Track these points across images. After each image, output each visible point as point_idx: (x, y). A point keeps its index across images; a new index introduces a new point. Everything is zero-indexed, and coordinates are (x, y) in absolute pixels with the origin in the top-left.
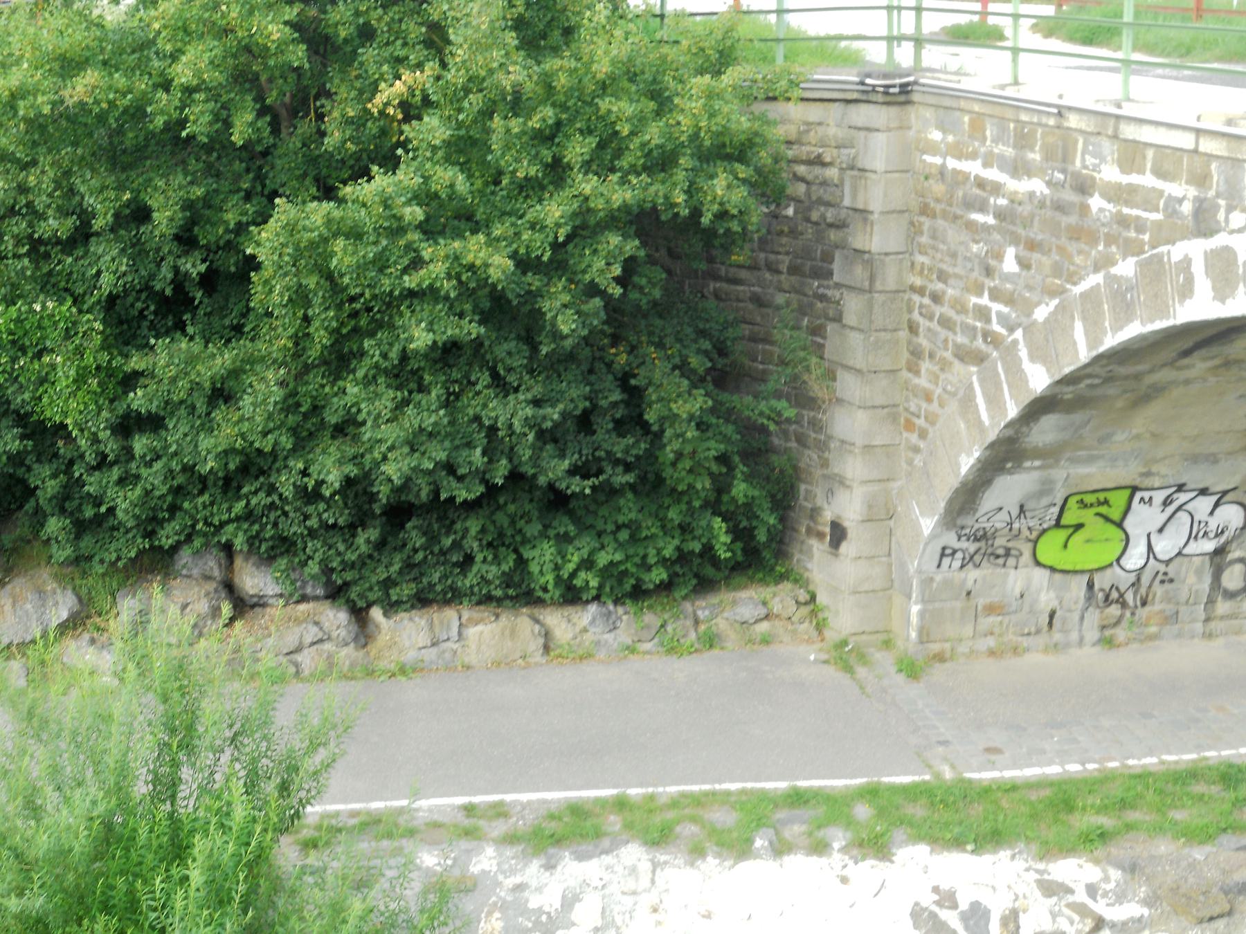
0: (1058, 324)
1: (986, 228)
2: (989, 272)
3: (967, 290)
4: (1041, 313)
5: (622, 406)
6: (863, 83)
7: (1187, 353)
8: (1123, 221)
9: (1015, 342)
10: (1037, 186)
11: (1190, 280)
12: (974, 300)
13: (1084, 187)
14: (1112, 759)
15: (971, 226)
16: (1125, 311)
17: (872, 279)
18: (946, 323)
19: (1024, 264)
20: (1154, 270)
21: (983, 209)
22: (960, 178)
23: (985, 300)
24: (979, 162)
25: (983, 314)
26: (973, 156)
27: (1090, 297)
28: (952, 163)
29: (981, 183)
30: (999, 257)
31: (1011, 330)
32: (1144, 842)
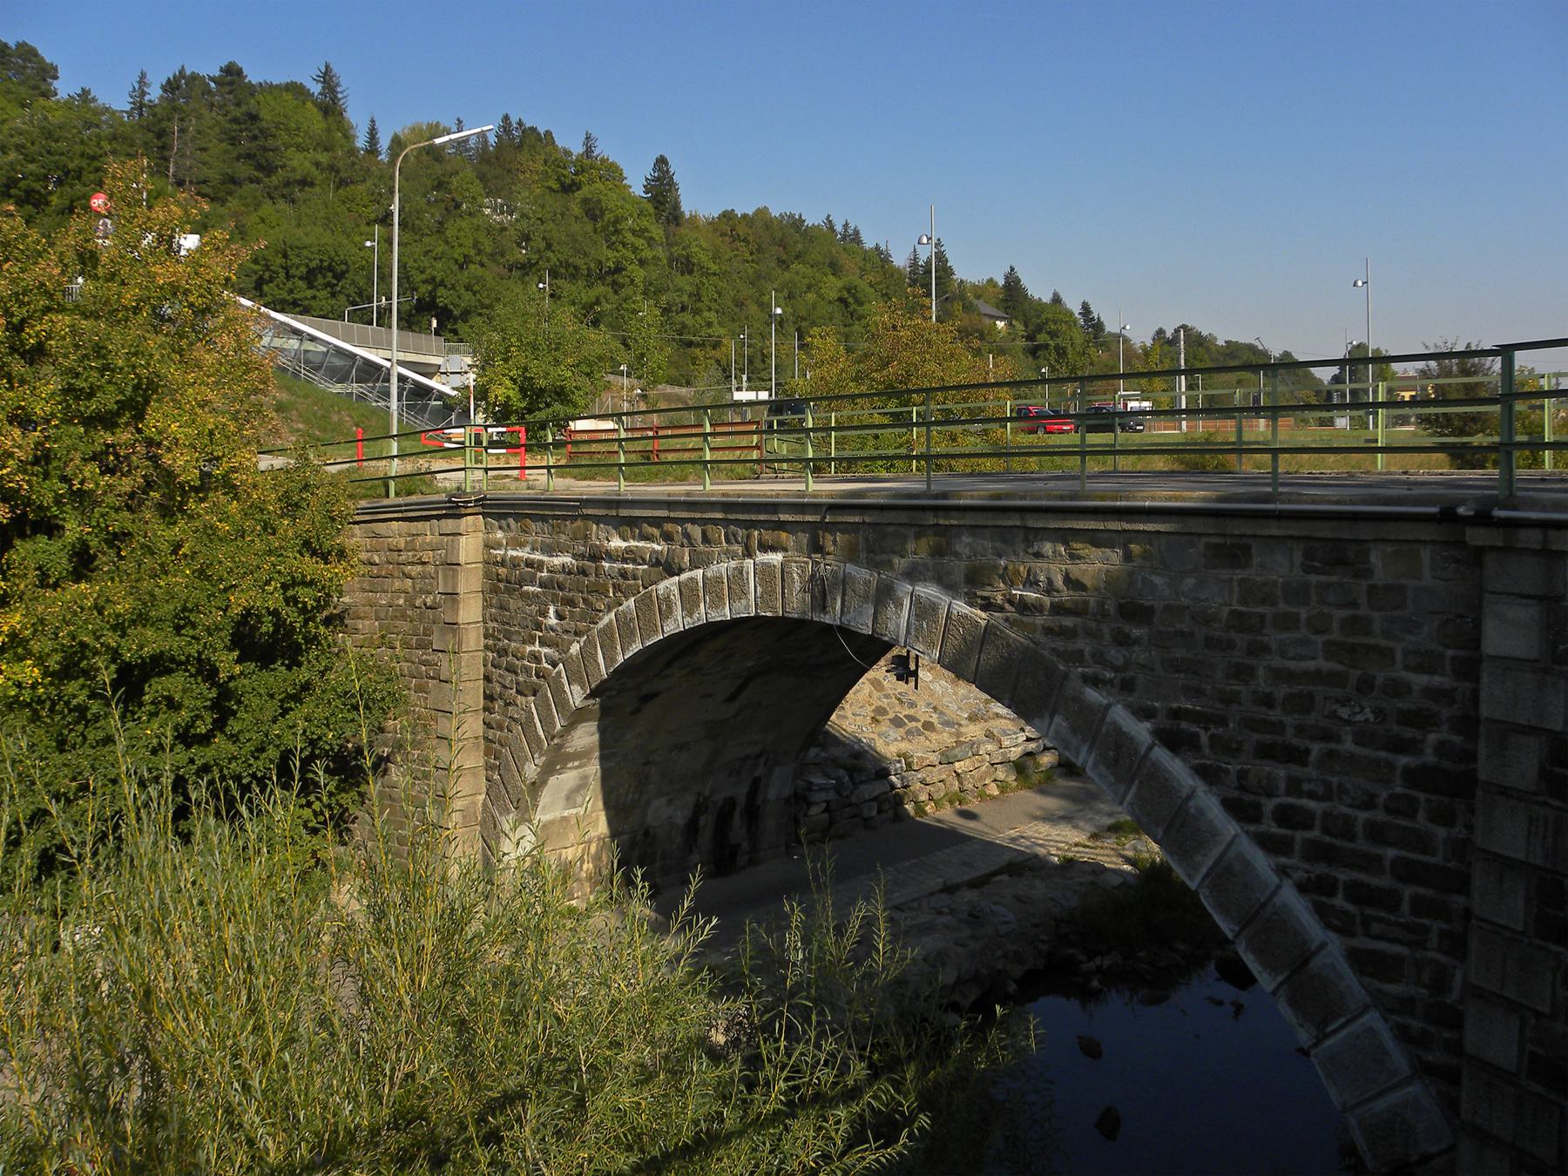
0: (587, 654)
1: (536, 595)
2: (538, 627)
3: (524, 642)
4: (575, 649)
5: (228, 729)
6: (450, 501)
7: (668, 665)
8: (624, 575)
9: (559, 673)
10: (567, 559)
11: (670, 608)
12: (528, 649)
13: (596, 556)
14: (430, 324)
15: (526, 596)
16: (627, 634)
17: (460, 645)
18: (511, 669)
19: (560, 617)
20: (645, 604)
21: (532, 583)
22: (515, 563)
23: (537, 647)
24: (528, 549)
25: (536, 658)
26: (522, 545)
27: (606, 633)
28: (511, 553)
29: (530, 563)
30: (544, 614)
31: (554, 665)
32: (611, 211)
